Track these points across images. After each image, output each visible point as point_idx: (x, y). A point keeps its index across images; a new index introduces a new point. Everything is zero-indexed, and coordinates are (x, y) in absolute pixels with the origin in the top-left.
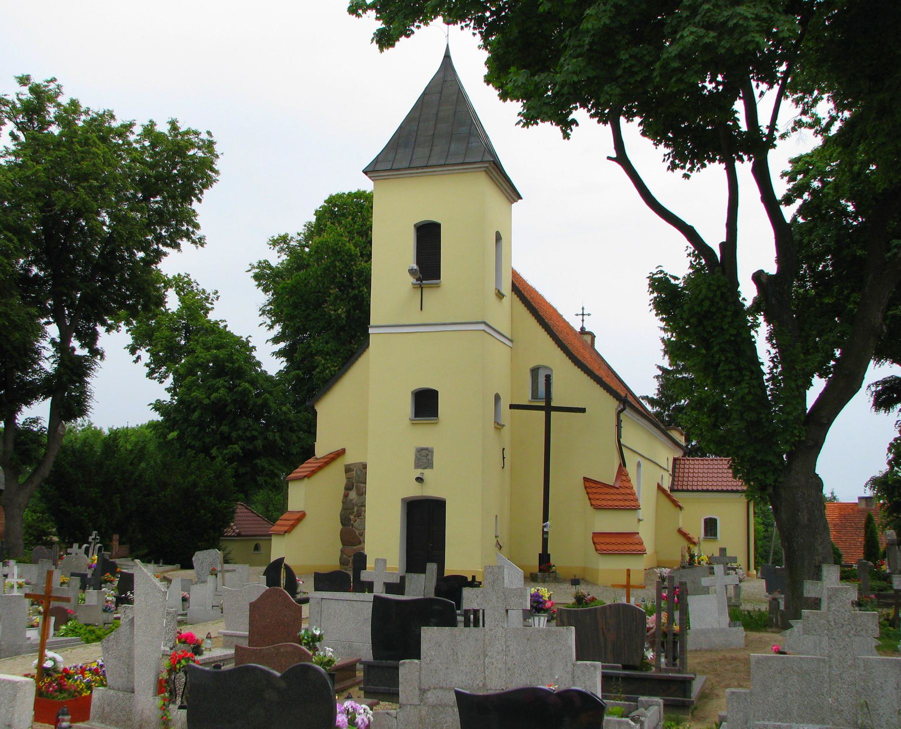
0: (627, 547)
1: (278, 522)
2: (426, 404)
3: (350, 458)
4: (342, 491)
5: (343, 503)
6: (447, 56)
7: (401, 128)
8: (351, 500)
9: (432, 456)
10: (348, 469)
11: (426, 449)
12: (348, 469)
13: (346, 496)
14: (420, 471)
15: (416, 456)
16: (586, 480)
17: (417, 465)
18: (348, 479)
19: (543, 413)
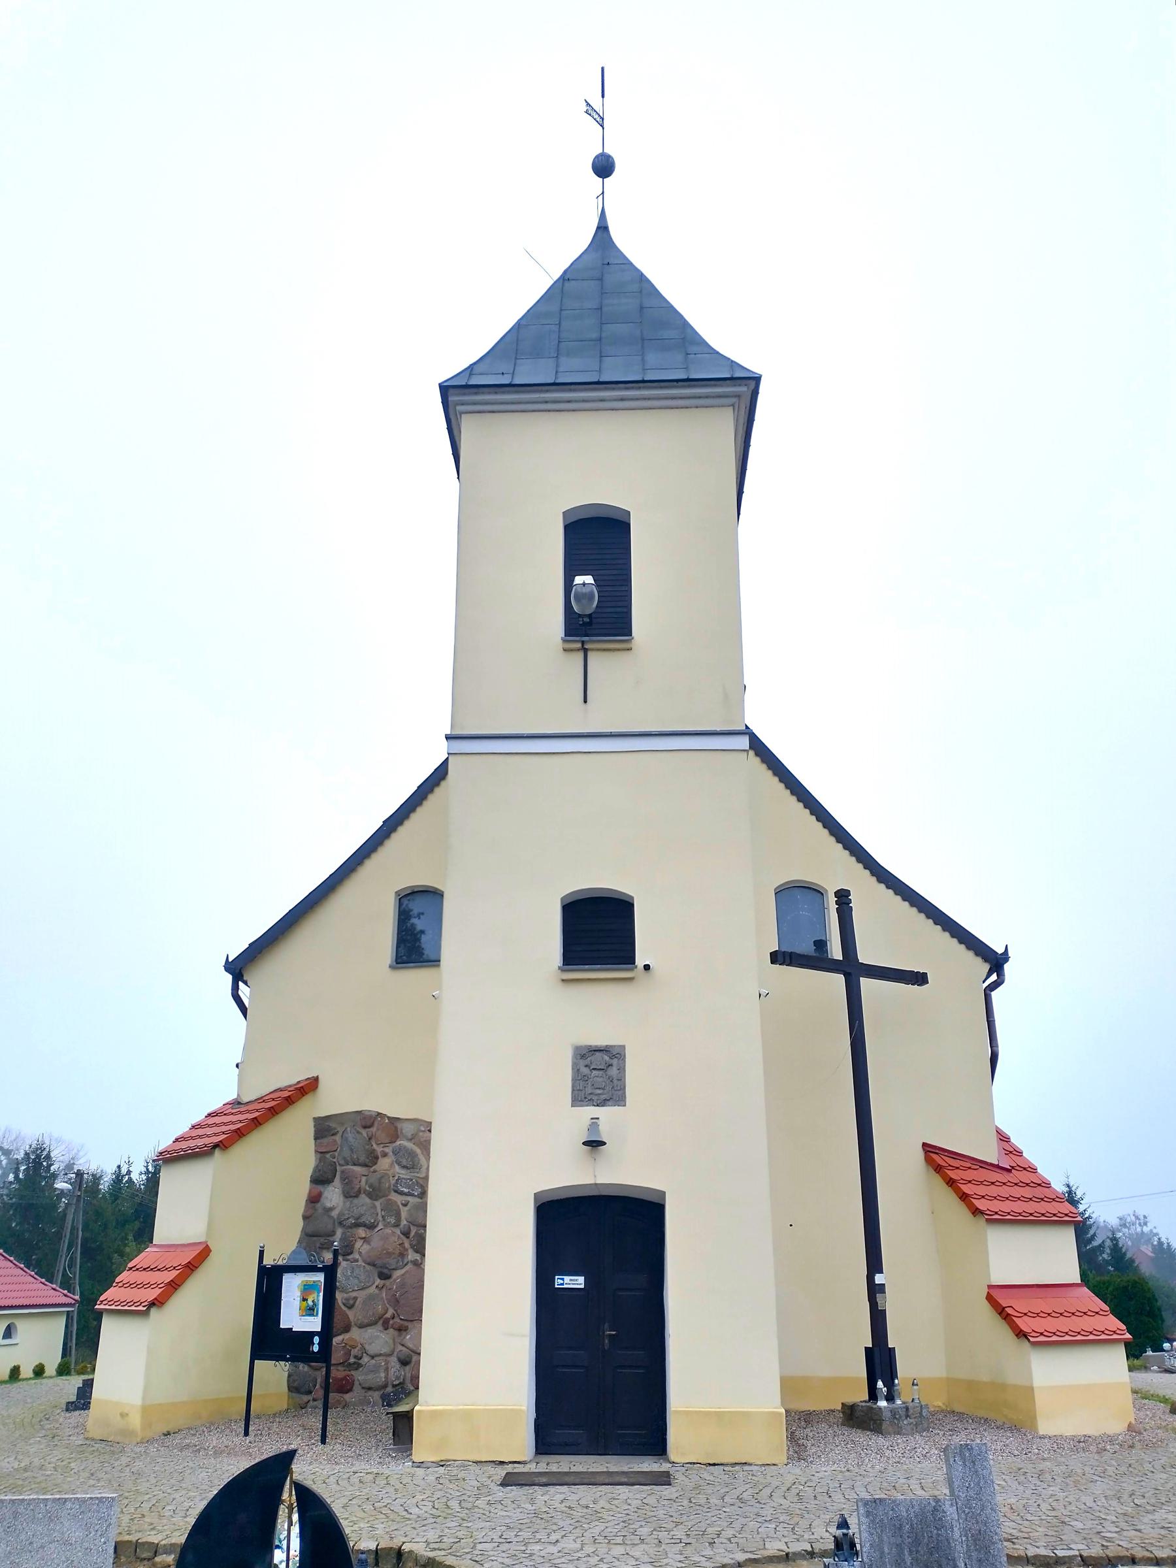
0: (1063, 1324)
1: (124, 1276)
2: (598, 932)
3: (334, 1100)
4: (303, 1188)
5: (305, 1218)
6: (603, 228)
7: (519, 326)
8: (329, 1210)
9: (622, 1069)
10: (324, 1128)
11: (605, 1050)
12: (324, 1128)
13: (314, 1199)
14: (590, 1111)
15: (576, 1070)
16: (924, 1145)
17: (580, 1097)
18: (321, 1154)
19: (840, 979)
